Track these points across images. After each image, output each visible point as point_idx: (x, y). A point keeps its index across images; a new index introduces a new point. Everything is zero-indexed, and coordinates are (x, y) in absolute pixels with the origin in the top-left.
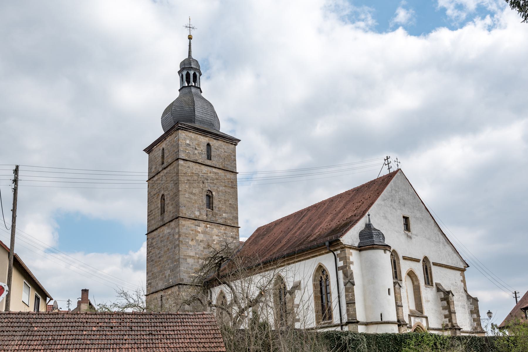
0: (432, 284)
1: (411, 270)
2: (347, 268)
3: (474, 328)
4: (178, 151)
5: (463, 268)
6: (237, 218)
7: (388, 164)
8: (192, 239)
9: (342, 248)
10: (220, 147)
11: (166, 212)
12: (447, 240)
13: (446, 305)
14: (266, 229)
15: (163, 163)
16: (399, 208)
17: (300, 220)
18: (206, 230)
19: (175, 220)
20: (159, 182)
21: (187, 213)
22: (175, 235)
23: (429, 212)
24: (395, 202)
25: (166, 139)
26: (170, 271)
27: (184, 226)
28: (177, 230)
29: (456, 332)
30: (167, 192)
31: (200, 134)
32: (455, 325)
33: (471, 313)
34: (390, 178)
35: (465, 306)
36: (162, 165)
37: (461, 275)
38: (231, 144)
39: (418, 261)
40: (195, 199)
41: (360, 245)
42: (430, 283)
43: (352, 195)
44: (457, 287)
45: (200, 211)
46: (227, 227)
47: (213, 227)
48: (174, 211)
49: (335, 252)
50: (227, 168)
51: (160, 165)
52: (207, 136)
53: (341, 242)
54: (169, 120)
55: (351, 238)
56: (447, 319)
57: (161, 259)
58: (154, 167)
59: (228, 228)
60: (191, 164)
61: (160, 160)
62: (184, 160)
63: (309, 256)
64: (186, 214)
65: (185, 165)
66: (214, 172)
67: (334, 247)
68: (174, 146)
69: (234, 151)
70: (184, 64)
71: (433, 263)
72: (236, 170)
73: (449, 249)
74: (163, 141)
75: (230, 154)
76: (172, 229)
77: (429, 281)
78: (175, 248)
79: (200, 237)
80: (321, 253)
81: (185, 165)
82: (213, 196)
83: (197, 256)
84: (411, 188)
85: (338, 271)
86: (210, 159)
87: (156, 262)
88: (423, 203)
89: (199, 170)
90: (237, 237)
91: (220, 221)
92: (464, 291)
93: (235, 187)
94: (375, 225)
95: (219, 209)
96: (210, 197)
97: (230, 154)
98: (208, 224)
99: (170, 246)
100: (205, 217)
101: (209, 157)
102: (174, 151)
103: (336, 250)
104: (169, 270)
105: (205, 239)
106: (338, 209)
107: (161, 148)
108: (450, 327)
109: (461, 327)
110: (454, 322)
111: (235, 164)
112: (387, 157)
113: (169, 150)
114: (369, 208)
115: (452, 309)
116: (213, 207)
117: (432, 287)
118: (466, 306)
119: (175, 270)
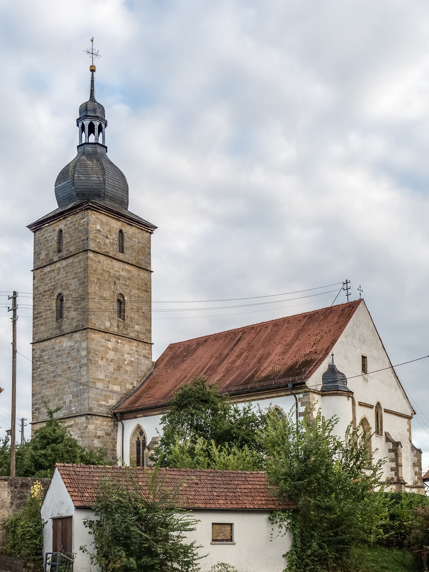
0: (382, 433)
1: (365, 418)
2: (310, 415)
3: (415, 482)
4: (87, 239)
5: (410, 415)
6: (150, 331)
7: (347, 289)
8: (102, 358)
9: (307, 392)
10: (134, 236)
11: (66, 318)
12: (399, 383)
13: (394, 457)
14: (185, 348)
15: (60, 251)
16: (359, 346)
17: (235, 345)
18: (117, 346)
19: (80, 332)
20: (53, 274)
21: (97, 324)
22: (80, 351)
23: (385, 351)
24: (356, 339)
25: (65, 218)
26: (73, 396)
27: (93, 340)
28: (84, 345)
29: (401, 487)
30: (67, 291)
31: (112, 217)
32: (401, 479)
33: (413, 466)
34: (351, 310)
35: (408, 457)
36: (58, 252)
37: (408, 424)
38: (146, 231)
39: (371, 407)
40: (105, 305)
41: (324, 390)
42: (380, 432)
43: (303, 322)
44: (403, 437)
45: (111, 321)
46: (139, 343)
47: (124, 342)
48: (79, 318)
49: (297, 396)
50: (141, 265)
51: (55, 252)
52: (120, 220)
53: (307, 385)
54: (68, 190)
55: (315, 381)
56: (393, 473)
57: (58, 379)
58: (43, 253)
59: (140, 344)
60: (101, 258)
61: (54, 244)
62: (94, 252)
63: (264, 397)
64: (95, 324)
65: (94, 258)
66: (126, 269)
67: (296, 390)
68: (79, 231)
69: (149, 241)
70: (86, 110)
71: (384, 409)
72: (150, 268)
73: (399, 393)
74: (61, 220)
75: (144, 245)
76: (76, 342)
77: (379, 431)
78: (81, 368)
79: (111, 355)
80: (280, 394)
81: (94, 258)
82: (124, 302)
83: (107, 379)
84: (371, 322)
85: (298, 417)
86: (123, 252)
87: (48, 382)
88: (381, 340)
89: (110, 266)
90: (150, 356)
91: (132, 335)
92: (409, 441)
93: (149, 290)
94: (339, 368)
95: (132, 319)
96: (121, 302)
97: (144, 245)
98: (119, 339)
99: (72, 363)
100: (116, 329)
101: (122, 250)
102: (80, 237)
103: (298, 393)
104: (70, 394)
105: (115, 359)
106: (289, 339)
107: (57, 229)
108: (395, 481)
109: (406, 481)
110: (400, 476)
111: (150, 259)
112: (347, 281)
113: (71, 234)
114: (332, 346)
115: (399, 462)
116: (124, 316)
117: (381, 436)
118: (410, 458)
119: (80, 395)
